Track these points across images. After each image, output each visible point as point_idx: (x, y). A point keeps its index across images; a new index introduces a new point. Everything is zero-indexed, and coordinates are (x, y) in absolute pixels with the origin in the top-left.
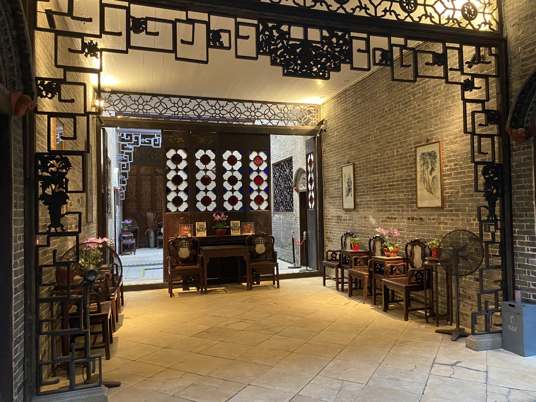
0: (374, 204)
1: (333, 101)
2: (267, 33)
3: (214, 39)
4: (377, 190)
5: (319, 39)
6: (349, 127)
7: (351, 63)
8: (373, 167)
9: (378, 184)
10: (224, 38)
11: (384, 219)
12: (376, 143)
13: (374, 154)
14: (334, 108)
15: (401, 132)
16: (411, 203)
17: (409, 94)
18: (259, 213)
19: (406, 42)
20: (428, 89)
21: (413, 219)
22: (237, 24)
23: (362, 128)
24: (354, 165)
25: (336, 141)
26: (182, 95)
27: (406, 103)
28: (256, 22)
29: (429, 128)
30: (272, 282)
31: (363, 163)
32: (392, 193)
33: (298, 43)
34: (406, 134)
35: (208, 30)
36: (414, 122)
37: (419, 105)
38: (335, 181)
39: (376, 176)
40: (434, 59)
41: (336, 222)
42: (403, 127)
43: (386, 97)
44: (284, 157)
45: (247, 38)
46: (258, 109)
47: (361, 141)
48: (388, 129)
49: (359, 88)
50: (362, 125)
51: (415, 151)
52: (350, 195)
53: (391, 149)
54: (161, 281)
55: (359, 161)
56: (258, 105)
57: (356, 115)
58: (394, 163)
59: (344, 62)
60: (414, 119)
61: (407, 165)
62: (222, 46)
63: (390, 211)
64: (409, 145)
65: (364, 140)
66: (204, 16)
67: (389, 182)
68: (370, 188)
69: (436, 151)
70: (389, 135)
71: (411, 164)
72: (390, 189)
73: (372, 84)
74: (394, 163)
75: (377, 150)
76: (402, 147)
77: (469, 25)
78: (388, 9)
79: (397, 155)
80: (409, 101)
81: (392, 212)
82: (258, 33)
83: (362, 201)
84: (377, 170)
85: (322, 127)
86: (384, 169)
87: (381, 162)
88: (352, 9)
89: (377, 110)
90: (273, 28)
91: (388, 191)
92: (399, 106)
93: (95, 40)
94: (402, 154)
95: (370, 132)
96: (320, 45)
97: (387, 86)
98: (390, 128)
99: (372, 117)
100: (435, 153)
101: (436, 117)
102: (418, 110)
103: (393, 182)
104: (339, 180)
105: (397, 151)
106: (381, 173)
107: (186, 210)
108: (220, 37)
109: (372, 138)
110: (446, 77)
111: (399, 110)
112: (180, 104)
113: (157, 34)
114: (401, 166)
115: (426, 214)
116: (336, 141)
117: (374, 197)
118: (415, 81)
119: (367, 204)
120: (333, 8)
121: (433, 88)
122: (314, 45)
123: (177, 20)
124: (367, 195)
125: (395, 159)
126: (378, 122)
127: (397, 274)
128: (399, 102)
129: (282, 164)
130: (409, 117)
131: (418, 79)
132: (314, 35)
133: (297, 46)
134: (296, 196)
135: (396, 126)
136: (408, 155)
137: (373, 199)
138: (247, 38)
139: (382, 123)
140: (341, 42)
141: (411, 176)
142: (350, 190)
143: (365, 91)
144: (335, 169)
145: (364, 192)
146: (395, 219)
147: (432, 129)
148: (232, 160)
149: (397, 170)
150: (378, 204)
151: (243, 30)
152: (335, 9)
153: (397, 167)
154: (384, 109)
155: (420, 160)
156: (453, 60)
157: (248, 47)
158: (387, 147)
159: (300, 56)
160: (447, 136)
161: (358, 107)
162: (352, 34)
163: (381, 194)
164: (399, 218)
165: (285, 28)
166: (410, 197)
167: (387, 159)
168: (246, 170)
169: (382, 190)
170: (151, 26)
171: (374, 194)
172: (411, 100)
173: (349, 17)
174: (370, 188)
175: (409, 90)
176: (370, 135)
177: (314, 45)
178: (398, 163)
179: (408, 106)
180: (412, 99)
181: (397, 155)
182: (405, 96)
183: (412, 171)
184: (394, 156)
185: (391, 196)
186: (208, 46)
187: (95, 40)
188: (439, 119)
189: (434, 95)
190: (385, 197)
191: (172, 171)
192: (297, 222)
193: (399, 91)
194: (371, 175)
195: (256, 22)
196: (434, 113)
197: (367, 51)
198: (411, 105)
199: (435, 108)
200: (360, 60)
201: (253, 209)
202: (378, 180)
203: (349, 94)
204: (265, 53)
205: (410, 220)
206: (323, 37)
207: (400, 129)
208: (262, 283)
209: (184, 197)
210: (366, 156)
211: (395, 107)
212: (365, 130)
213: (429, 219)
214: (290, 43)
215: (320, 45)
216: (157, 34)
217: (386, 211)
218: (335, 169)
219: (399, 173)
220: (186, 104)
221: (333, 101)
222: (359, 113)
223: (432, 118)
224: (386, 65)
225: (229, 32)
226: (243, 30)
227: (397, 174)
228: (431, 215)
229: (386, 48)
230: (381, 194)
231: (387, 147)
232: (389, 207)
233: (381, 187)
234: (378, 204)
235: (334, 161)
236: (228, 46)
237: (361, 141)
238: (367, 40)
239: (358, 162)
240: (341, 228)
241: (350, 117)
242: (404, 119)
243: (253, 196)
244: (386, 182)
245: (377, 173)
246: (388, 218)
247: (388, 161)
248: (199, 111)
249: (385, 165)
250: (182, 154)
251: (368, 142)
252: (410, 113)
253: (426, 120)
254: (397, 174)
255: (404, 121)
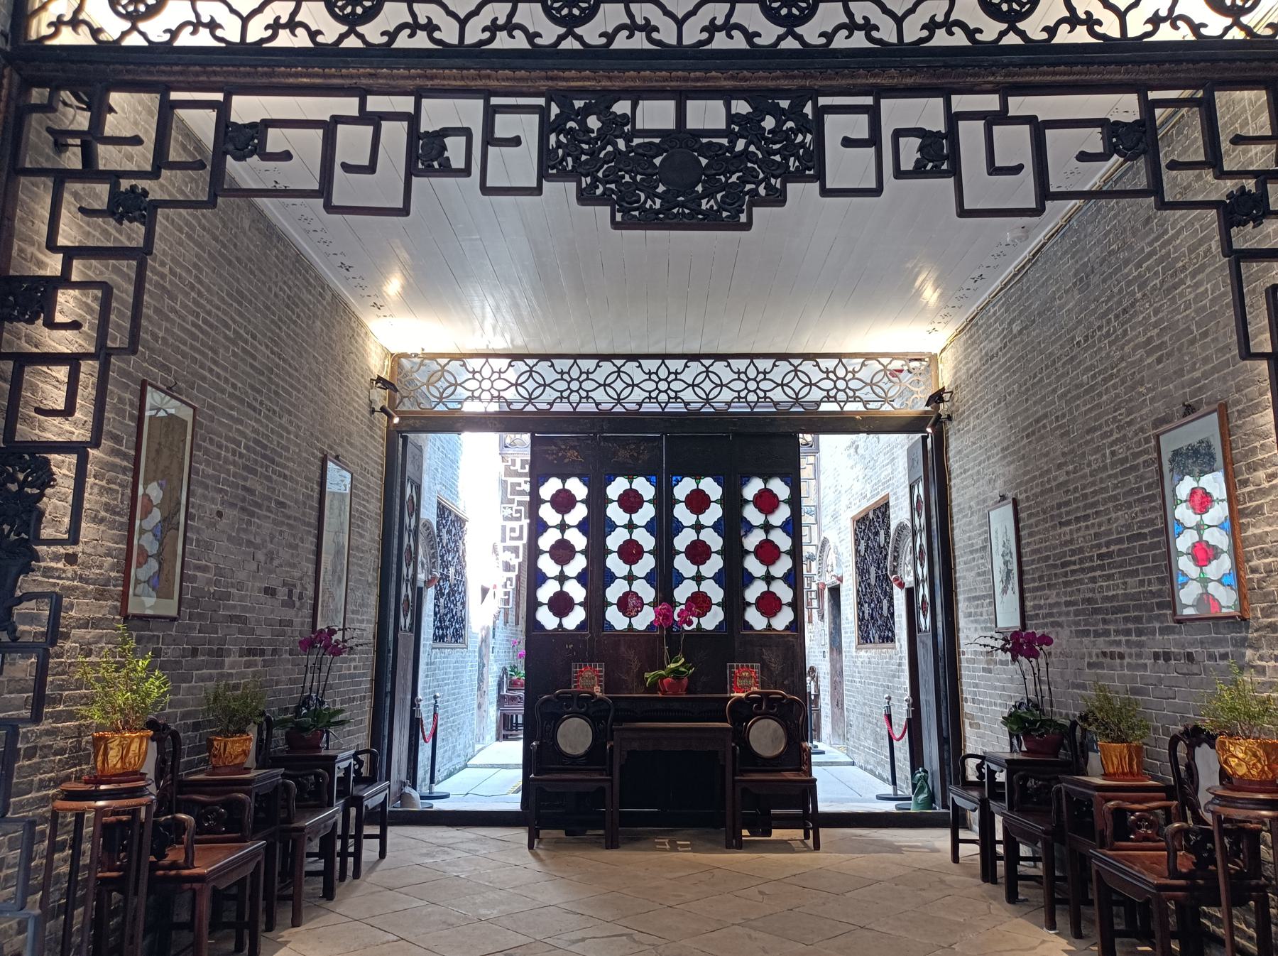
0: (1068, 614)
1: (963, 338)
2: (571, 124)
3: (426, 154)
4: (1073, 572)
5: (722, 125)
6: (999, 402)
7: (820, 177)
8: (1059, 506)
9: (1073, 553)
10: (455, 149)
11: (1094, 659)
12: (1062, 435)
13: (1060, 466)
14: (965, 358)
15: (1117, 396)
16: (1161, 606)
17: (1129, 284)
18: (769, 635)
19: (1004, 104)
20: (1177, 259)
21: (1167, 656)
22: (490, 114)
23: (1027, 400)
24: (1015, 503)
25: (974, 443)
26: (578, 352)
27: (1125, 311)
28: (541, 101)
29: (1189, 372)
30: (799, 833)
31: (1036, 496)
32: (1110, 577)
33: (657, 140)
34: (1130, 400)
35: (414, 133)
36: (1149, 361)
37: (1156, 312)
38: (976, 551)
39: (1067, 529)
40: (1106, 139)
41: (984, 670)
42: (1123, 381)
43: (1075, 305)
44: (873, 497)
45: (516, 141)
46: (765, 373)
47: (1028, 436)
48: (1086, 392)
49: (1014, 293)
50: (1028, 390)
51: (1158, 448)
52: (1010, 591)
53: (1098, 450)
54: (514, 804)
55: (1026, 491)
56: (764, 364)
57: (1012, 366)
58: (1105, 490)
59: (799, 177)
60: (1149, 354)
61: (1139, 490)
62: (447, 170)
63: (1106, 633)
64: (1142, 430)
65: (1033, 433)
66: (405, 104)
67: (1099, 546)
68: (1055, 566)
69: (1212, 440)
70: (1090, 410)
71: (1149, 487)
72: (1102, 567)
73: (1042, 276)
74: (1105, 490)
75: (1064, 454)
76: (1124, 438)
77: (1235, 29)
78: (940, 18)
79: (1113, 465)
80: (1133, 305)
81: (1113, 638)
82: (546, 128)
83: (1040, 607)
84: (1068, 513)
85: (944, 408)
86: (1086, 507)
87: (1076, 489)
88: (822, 35)
89: (1058, 345)
90: (586, 111)
91: (1098, 573)
92: (1109, 322)
93: (142, 184)
94: (1125, 460)
95: (1045, 407)
96: (725, 141)
97: (1075, 275)
98: (1092, 388)
99: (1047, 367)
100: (1209, 446)
101: (1205, 335)
102: (1155, 325)
103: (1108, 544)
104: (984, 548)
105: (1113, 453)
106: (1078, 519)
107: (582, 626)
108: (444, 148)
109: (1051, 423)
110: (1155, 189)
111: (1108, 335)
112: (575, 373)
113: (287, 156)
114: (1126, 494)
115: (1202, 642)
116: (974, 443)
117: (1065, 594)
118: (1038, 211)
119: (1051, 615)
120: (765, 40)
121: (1191, 251)
122: (704, 140)
123: (337, 120)
124: (1050, 586)
125: (1110, 476)
126: (1063, 375)
127: (1146, 838)
128: (1105, 314)
129: (871, 516)
130: (1134, 350)
131: (1048, 204)
132: (707, 115)
133: (658, 150)
134: (899, 597)
135: (1105, 380)
136: (1141, 460)
137: (1064, 599)
138: (516, 141)
139: (1072, 379)
140: (790, 124)
141: (1152, 522)
142: (1009, 572)
143: (1027, 299)
144: (975, 518)
145: (1041, 578)
146: (1121, 656)
147: (1197, 374)
148: (698, 502)
149: (1117, 509)
150: (1077, 613)
151: (505, 125)
152: (772, 40)
153: (1115, 498)
154: (1073, 338)
155: (1171, 470)
156: (1185, 140)
157: (518, 165)
158: (1087, 443)
159: (663, 174)
160: (1239, 390)
161: (1016, 344)
162: (823, 101)
163: (1080, 582)
164: (1130, 655)
165: (622, 107)
166: (1154, 588)
167: (1090, 479)
168: (732, 526)
169: (1082, 570)
170: (276, 140)
171: (1066, 584)
172: (1136, 301)
173: (820, 58)
174: (1055, 566)
175: (1128, 275)
176: (1045, 416)
177: (704, 140)
178: (1116, 487)
179: (1129, 320)
180: (1139, 295)
181: (1113, 465)
182: (1120, 291)
183: (1153, 509)
184: (1105, 468)
185: (1108, 588)
186: (411, 172)
187: (142, 184)
188: (1213, 340)
189: (1193, 275)
190: (1093, 590)
191: (550, 530)
192: (903, 671)
193: (1104, 281)
194: (1054, 527)
195: (541, 101)
196: (1199, 325)
197: (874, 140)
198: (1136, 314)
199: (1197, 312)
200: (845, 166)
201: (751, 628)
202: (1071, 542)
203: (995, 313)
204: (563, 175)
205: (1161, 661)
206: (731, 118)
207: (1115, 387)
208: (777, 834)
209: (577, 592)
210: (1041, 476)
211: (1100, 328)
212: (1035, 403)
213: (1211, 657)
214: (636, 141)
215: (725, 141)
216: (287, 156)
217: (1097, 634)
218: (975, 518)
219: (1122, 517)
220: (676, 373)
221: (963, 338)
222: (1018, 360)
223: (1193, 342)
224: (937, 173)
225: (467, 132)
226: (505, 125)
227: (1117, 519)
228: (1217, 643)
229: (939, 125)
230: (1080, 582)
231: (1087, 443)
232: (1105, 621)
233: (1081, 561)
234: (1077, 613)
235: (971, 499)
236: (462, 166)
237: (1028, 436)
238: (874, 114)
239: (1024, 495)
240: (995, 688)
241: (1001, 375)
242: (1122, 359)
243: (752, 594)
244: (1092, 547)
245: (1068, 523)
246: (1104, 654)
247: (1093, 484)
248: (796, 385)
249: (1085, 496)
250: (577, 488)
251: (1042, 437)
252: (1137, 337)
253: (1180, 350)
254: (1117, 519)
255: (1124, 364)
